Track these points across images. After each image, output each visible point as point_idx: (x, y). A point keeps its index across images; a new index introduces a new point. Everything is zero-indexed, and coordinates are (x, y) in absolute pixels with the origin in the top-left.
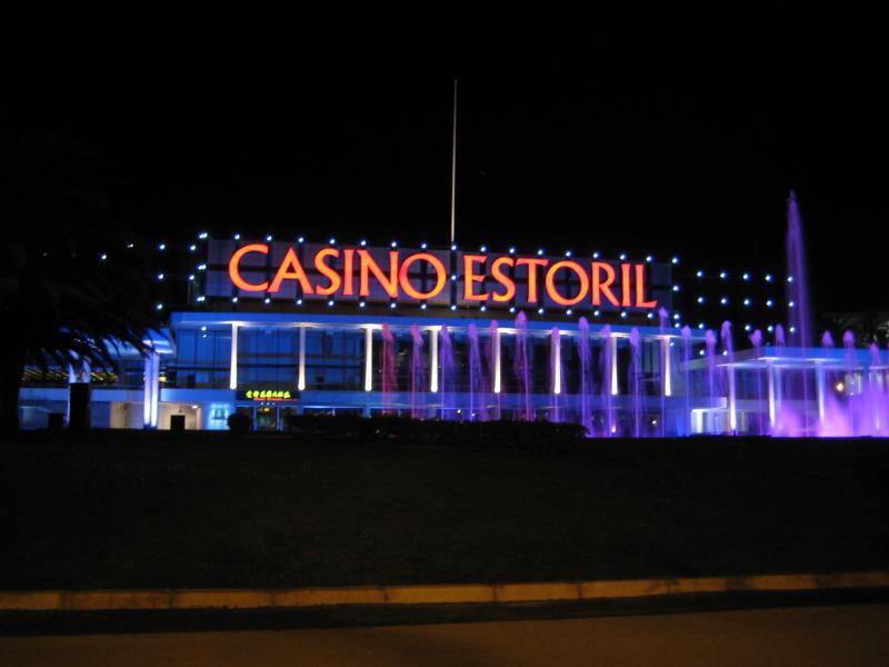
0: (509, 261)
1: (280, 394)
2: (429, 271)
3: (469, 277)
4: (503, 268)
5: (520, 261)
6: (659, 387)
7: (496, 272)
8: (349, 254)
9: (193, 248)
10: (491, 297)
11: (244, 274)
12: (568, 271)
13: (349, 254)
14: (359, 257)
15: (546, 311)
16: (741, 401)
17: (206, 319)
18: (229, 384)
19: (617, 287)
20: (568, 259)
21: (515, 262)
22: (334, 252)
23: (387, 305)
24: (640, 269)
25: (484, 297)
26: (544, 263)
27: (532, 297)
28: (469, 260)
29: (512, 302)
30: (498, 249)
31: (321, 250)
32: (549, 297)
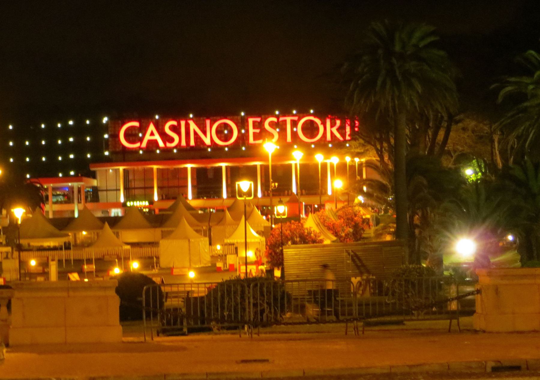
0: (275, 119)
2: (315, 125)
3: (251, 131)
4: (271, 124)
5: (281, 119)
8: (183, 123)
9: (71, 123)
12: (312, 122)
13: (183, 123)
17: (112, 166)
20: (311, 115)
26: (296, 118)
28: (251, 121)
31: (268, 117)
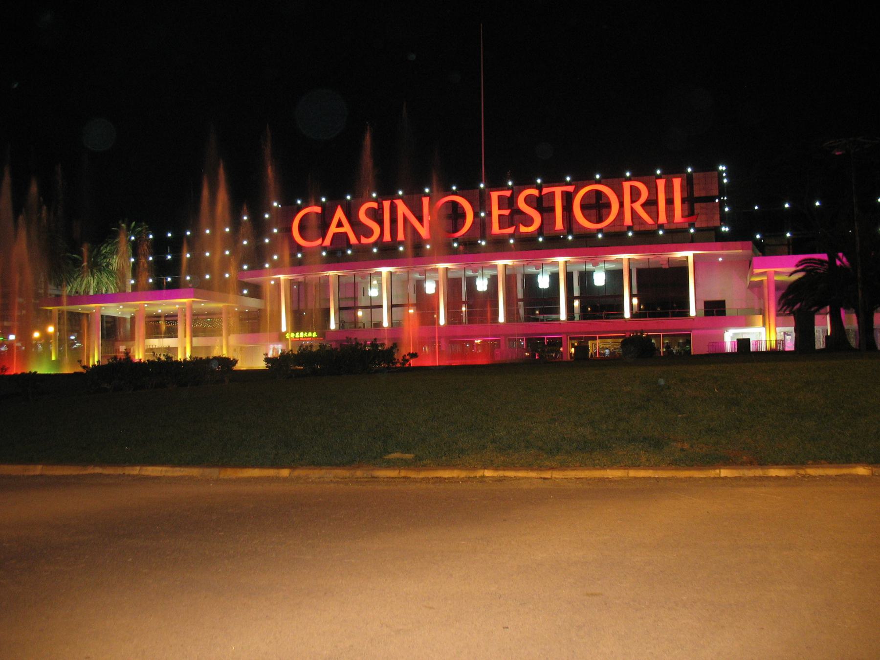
0: (535, 192)
1: (310, 334)
2: (459, 211)
3: (496, 212)
5: (545, 191)
6: (435, 321)
7: (522, 205)
8: (387, 204)
10: (517, 228)
11: (586, 212)
13: (387, 204)
14: (396, 207)
15: (575, 237)
16: (780, 318)
18: (623, 314)
19: (651, 204)
21: (540, 192)
22: (375, 205)
23: (624, 234)
24: (677, 182)
25: (511, 230)
27: (559, 225)
28: (495, 195)
29: (540, 231)
30: (524, 181)
32: (577, 223)
